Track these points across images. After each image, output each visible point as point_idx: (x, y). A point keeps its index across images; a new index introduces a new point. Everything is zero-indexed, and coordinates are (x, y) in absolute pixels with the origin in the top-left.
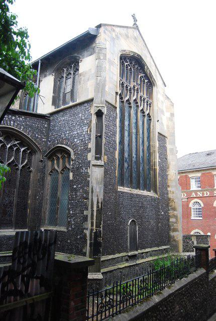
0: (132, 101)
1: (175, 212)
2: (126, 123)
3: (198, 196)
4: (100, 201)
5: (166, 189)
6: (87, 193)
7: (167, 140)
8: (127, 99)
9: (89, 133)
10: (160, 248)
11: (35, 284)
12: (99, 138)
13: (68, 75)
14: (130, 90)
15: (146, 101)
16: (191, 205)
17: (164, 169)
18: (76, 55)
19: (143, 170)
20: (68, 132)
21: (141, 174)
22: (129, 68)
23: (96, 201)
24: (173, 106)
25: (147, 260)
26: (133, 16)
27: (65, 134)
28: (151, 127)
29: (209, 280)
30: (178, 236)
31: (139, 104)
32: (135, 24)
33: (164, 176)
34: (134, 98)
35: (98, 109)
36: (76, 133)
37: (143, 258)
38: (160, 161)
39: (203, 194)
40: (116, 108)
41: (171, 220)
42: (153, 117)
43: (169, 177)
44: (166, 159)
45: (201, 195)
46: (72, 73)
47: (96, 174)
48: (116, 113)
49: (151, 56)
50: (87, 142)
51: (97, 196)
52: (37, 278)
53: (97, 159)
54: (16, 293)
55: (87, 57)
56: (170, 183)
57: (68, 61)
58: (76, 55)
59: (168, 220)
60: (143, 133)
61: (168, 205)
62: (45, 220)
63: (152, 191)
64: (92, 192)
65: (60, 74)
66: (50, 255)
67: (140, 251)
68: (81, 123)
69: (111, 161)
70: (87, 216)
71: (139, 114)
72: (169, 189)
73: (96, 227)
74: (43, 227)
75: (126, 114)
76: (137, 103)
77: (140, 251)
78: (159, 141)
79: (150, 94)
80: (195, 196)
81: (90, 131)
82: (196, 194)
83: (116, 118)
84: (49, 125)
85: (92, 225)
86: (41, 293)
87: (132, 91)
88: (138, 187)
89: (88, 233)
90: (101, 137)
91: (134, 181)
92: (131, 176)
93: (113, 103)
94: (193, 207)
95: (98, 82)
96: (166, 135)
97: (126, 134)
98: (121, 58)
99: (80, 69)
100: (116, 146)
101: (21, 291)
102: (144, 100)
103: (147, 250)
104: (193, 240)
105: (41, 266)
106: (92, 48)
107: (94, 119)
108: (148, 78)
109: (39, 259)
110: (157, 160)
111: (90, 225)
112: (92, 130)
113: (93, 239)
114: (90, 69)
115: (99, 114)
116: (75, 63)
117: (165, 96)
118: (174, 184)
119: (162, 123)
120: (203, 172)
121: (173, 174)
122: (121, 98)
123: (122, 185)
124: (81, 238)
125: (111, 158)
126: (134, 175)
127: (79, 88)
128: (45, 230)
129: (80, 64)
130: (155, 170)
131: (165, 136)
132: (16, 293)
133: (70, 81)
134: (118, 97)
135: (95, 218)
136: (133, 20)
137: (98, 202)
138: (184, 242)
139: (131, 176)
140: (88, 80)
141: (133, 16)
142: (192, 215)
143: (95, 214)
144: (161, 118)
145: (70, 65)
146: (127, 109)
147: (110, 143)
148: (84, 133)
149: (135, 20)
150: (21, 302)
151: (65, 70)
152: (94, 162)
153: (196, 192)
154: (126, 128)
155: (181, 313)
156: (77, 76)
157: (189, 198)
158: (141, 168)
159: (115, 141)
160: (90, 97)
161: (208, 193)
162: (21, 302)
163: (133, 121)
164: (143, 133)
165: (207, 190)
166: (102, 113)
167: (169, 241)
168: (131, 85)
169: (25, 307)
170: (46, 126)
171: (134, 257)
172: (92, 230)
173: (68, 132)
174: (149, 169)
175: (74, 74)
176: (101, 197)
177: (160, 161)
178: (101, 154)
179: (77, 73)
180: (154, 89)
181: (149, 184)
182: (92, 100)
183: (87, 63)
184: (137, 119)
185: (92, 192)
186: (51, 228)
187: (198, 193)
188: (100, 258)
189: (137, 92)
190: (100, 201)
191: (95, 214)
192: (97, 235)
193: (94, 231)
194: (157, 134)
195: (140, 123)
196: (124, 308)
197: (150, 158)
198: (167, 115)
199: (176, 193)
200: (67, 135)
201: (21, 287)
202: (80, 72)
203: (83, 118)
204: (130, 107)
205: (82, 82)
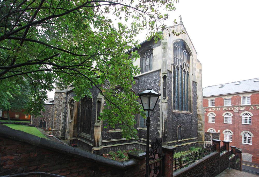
0: (179, 67)
1: (201, 121)
2: (176, 78)
3: (213, 110)
4: (166, 118)
5: (196, 110)
6: (159, 114)
7: (197, 85)
8: (177, 66)
9: (159, 86)
10: (193, 139)
11: (157, 155)
12: (164, 89)
13: (147, 56)
14: (178, 61)
15: (186, 65)
16: (208, 115)
17: (196, 98)
18: (151, 46)
19: (185, 101)
20: (148, 85)
21: (184, 103)
22: (178, 48)
23: (164, 118)
24: (201, 65)
25: (186, 144)
26: (180, 17)
27: (147, 86)
28: (189, 78)
29: (220, 156)
30: (202, 133)
31: (183, 67)
32: (181, 21)
33: (195, 103)
34: (180, 65)
35: (164, 75)
36: (153, 86)
37: (184, 143)
38: (193, 96)
39: (216, 109)
40: (172, 72)
41: (198, 125)
42: (190, 73)
43: (198, 104)
44: (197, 94)
45: (215, 110)
46: (149, 55)
47: (163, 107)
48: (172, 75)
49: (190, 39)
50: (158, 90)
51: (165, 116)
52: (157, 154)
53: (164, 99)
54: (152, 159)
55: (157, 47)
56: (198, 106)
57: (146, 49)
58: (151, 46)
59: (197, 125)
60: (185, 82)
61: (197, 118)
62: (139, 125)
63: (189, 111)
64: (162, 114)
65: (143, 56)
66: (160, 145)
67: (183, 140)
68: (155, 81)
69: (170, 99)
70: (159, 124)
71: (183, 73)
72: (198, 110)
73: (164, 129)
74: (138, 127)
75: (176, 74)
76: (182, 67)
77: (183, 140)
78: (193, 85)
79: (189, 60)
80: (211, 110)
81: (160, 85)
82: (212, 109)
83: (172, 77)
84: (139, 82)
85: (163, 129)
86: (158, 159)
87: (179, 61)
88: (182, 109)
89: (160, 132)
90: (165, 88)
91: (180, 107)
92: (178, 104)
93: (170, 70)
94: (210, 116)
95: (163, 61)
96: (197, 82)
97: (176, 84)
98: (174, 44)
99: (153, 53)
100: (172, 92)
101: (153, 158)
102: (185, 64)
103: (186, 140)
104: (210, 135)
105: (158, 149)
106: (159, 42)
107: (162, 80)
108: (188, 52)
109: (157, 147)
110: (192, 95)
111: (162, 129)
112: (161, 85)
113: (163, 135)
114: (159, 54)
115: (165, 77)
116: (151, 50)
117: (197, 60)
118: (200, 107)
119: (195, 75)
120: (217, 97)
121: (200, 102)
122: (174, 66)
123: (175, 109)
124: (156, 133)
125: (170, 97)
126: (180, 104)
127: (154, 63)
128: (139, 129)
129: (153, 51)
130: (190, 101)
131: (196, 82)
132: (152, 159)
133: (148, 60)
134: (173, 66)
135: (164, 126)
136: (180, 19)
137: (165, 119)
138: (205, 136)
139: (178, 104)
140: (158, 59)
141: (180, 17)
142: (209, 121)
143: (164, 124)
144: (194, 73)
145: (148, 50)
146: (176, 71)
147: (169, 90)
148: (157, 86)
149: (181, 19)
150: (154, 161)
151: (145, 53)
152: (163, 100)
153: (211, 108)
154: (176, 81)
155: (207, 170)
156: (151, 57)
157: (208, 112)
158: (183, 100)
159: (171, 89)
160: (159, 68)
161: (220, 109)
162: (154, 161)
163: (180, 77)
164: (185, 82)
165: (218, 107)
166: (166, 77)
167: (197, 135)
168: (179, 58)
169: (155, 163)
170: (137, 82)
171: (181, 142)
172: (162, 131)
173: (148, 85)
174: (187, 100)
175: (150, 56)
176: (166, 116)
177: (193, 96)
178: (166, 97)
179: (151, 55)
180: (191, 57)
181: (188, 108)
182: (160, 70)
183: (157, 51)
184: (181, 76)
185: (162, 114)
186: (141, 128)
187: (213, 109)
188: (166, 143)
189: (182, 61)
190: (166, 118)
191: (164, 124)
192: (165, 133)
193: (164, 131)
194: (192, 82)
195: (183, 77)
196: (184, 166)
197: (188, 94)
198: (198, 70)
199: (200, 111)
200: (148, 87)
201: (154, 157)
202: (153, 55)
203: (156, 79)
204: (178, 70)
205: (155, 61)
